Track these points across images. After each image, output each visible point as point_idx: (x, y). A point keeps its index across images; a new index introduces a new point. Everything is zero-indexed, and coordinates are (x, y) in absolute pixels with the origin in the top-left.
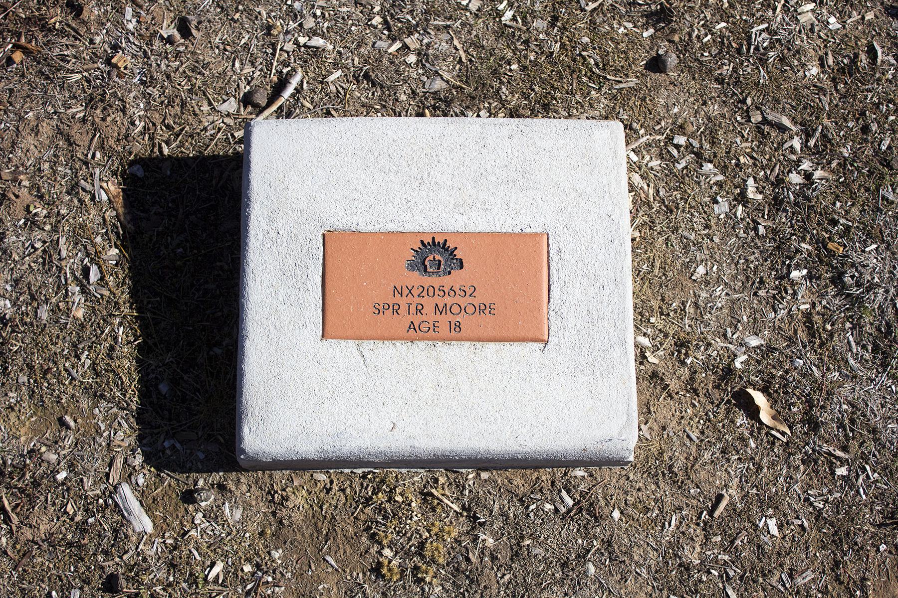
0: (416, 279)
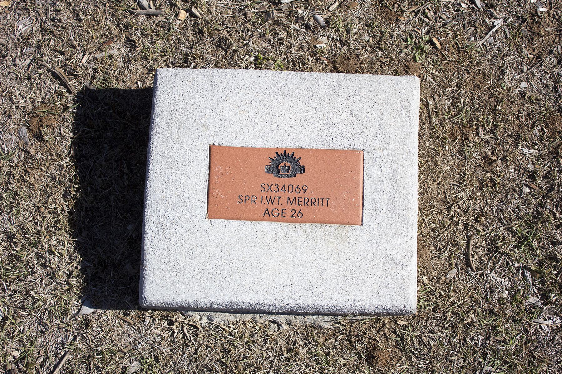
0: (272, 179)
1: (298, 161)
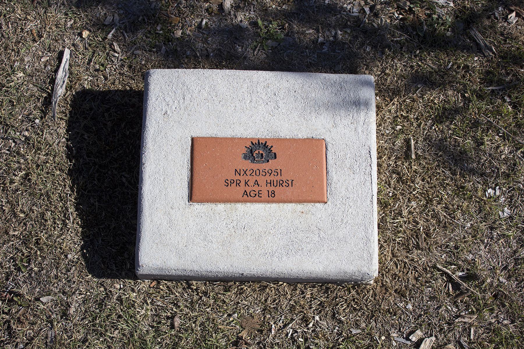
0: (248, 165)
1: (270, 148)
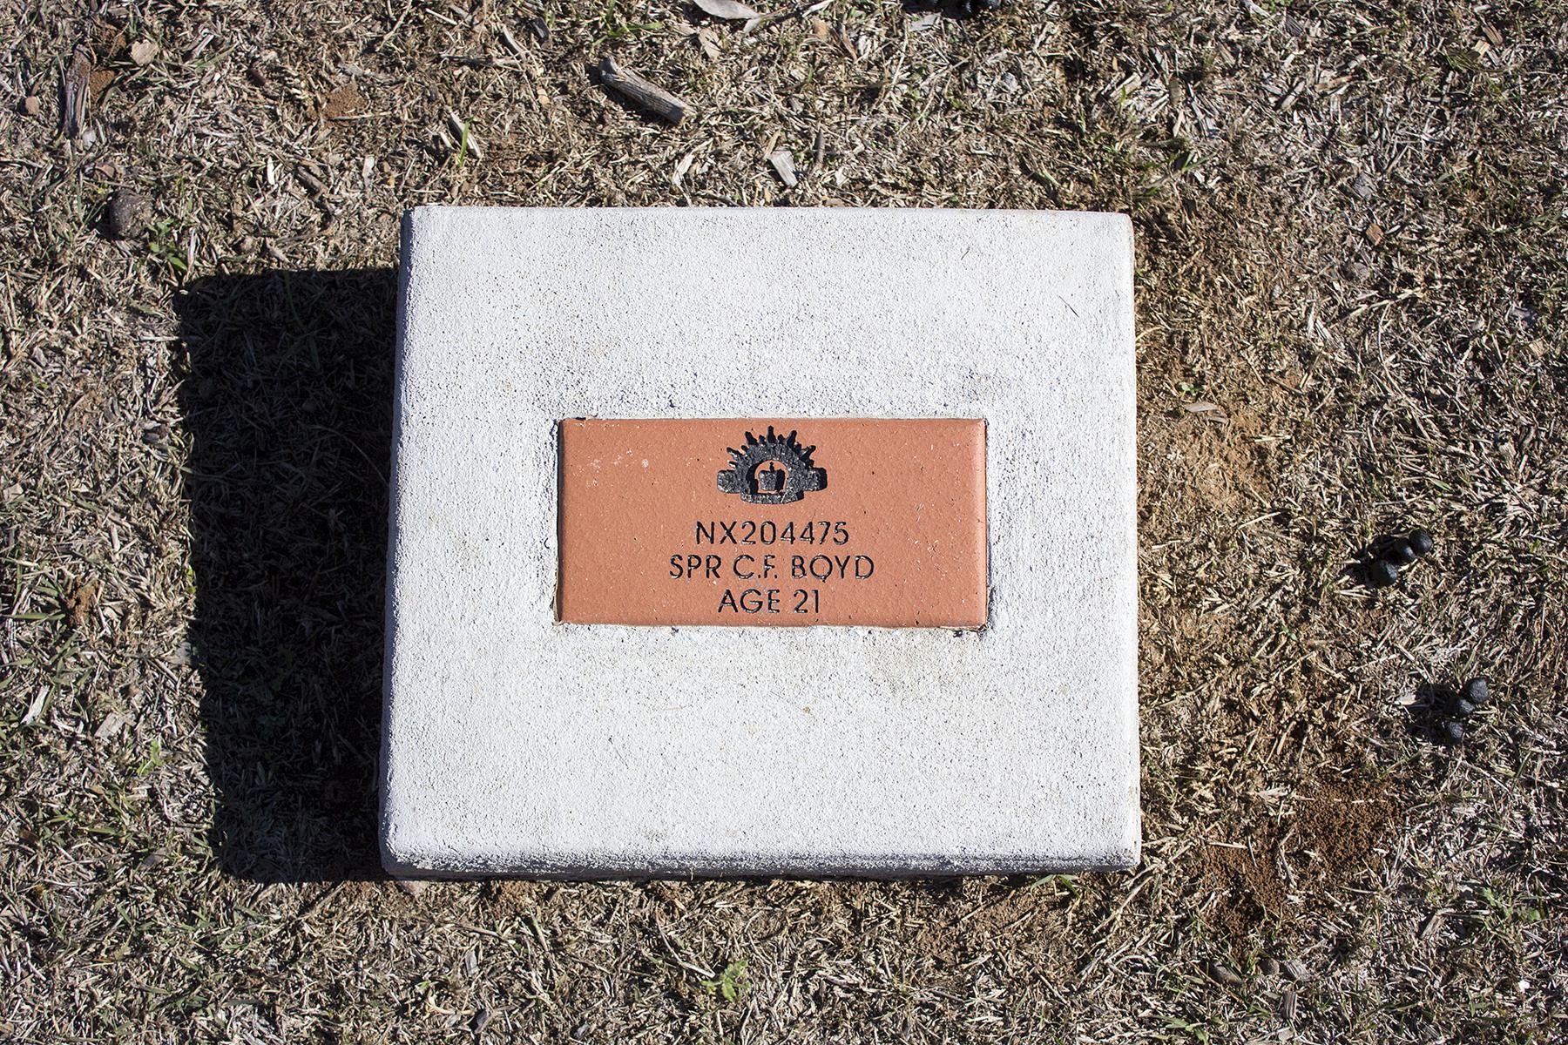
0: (738, 508)
